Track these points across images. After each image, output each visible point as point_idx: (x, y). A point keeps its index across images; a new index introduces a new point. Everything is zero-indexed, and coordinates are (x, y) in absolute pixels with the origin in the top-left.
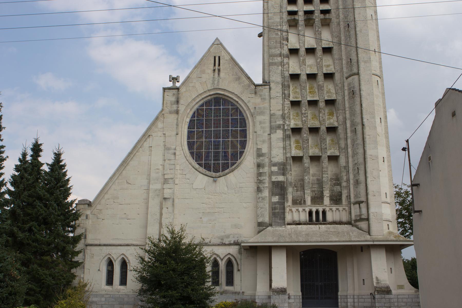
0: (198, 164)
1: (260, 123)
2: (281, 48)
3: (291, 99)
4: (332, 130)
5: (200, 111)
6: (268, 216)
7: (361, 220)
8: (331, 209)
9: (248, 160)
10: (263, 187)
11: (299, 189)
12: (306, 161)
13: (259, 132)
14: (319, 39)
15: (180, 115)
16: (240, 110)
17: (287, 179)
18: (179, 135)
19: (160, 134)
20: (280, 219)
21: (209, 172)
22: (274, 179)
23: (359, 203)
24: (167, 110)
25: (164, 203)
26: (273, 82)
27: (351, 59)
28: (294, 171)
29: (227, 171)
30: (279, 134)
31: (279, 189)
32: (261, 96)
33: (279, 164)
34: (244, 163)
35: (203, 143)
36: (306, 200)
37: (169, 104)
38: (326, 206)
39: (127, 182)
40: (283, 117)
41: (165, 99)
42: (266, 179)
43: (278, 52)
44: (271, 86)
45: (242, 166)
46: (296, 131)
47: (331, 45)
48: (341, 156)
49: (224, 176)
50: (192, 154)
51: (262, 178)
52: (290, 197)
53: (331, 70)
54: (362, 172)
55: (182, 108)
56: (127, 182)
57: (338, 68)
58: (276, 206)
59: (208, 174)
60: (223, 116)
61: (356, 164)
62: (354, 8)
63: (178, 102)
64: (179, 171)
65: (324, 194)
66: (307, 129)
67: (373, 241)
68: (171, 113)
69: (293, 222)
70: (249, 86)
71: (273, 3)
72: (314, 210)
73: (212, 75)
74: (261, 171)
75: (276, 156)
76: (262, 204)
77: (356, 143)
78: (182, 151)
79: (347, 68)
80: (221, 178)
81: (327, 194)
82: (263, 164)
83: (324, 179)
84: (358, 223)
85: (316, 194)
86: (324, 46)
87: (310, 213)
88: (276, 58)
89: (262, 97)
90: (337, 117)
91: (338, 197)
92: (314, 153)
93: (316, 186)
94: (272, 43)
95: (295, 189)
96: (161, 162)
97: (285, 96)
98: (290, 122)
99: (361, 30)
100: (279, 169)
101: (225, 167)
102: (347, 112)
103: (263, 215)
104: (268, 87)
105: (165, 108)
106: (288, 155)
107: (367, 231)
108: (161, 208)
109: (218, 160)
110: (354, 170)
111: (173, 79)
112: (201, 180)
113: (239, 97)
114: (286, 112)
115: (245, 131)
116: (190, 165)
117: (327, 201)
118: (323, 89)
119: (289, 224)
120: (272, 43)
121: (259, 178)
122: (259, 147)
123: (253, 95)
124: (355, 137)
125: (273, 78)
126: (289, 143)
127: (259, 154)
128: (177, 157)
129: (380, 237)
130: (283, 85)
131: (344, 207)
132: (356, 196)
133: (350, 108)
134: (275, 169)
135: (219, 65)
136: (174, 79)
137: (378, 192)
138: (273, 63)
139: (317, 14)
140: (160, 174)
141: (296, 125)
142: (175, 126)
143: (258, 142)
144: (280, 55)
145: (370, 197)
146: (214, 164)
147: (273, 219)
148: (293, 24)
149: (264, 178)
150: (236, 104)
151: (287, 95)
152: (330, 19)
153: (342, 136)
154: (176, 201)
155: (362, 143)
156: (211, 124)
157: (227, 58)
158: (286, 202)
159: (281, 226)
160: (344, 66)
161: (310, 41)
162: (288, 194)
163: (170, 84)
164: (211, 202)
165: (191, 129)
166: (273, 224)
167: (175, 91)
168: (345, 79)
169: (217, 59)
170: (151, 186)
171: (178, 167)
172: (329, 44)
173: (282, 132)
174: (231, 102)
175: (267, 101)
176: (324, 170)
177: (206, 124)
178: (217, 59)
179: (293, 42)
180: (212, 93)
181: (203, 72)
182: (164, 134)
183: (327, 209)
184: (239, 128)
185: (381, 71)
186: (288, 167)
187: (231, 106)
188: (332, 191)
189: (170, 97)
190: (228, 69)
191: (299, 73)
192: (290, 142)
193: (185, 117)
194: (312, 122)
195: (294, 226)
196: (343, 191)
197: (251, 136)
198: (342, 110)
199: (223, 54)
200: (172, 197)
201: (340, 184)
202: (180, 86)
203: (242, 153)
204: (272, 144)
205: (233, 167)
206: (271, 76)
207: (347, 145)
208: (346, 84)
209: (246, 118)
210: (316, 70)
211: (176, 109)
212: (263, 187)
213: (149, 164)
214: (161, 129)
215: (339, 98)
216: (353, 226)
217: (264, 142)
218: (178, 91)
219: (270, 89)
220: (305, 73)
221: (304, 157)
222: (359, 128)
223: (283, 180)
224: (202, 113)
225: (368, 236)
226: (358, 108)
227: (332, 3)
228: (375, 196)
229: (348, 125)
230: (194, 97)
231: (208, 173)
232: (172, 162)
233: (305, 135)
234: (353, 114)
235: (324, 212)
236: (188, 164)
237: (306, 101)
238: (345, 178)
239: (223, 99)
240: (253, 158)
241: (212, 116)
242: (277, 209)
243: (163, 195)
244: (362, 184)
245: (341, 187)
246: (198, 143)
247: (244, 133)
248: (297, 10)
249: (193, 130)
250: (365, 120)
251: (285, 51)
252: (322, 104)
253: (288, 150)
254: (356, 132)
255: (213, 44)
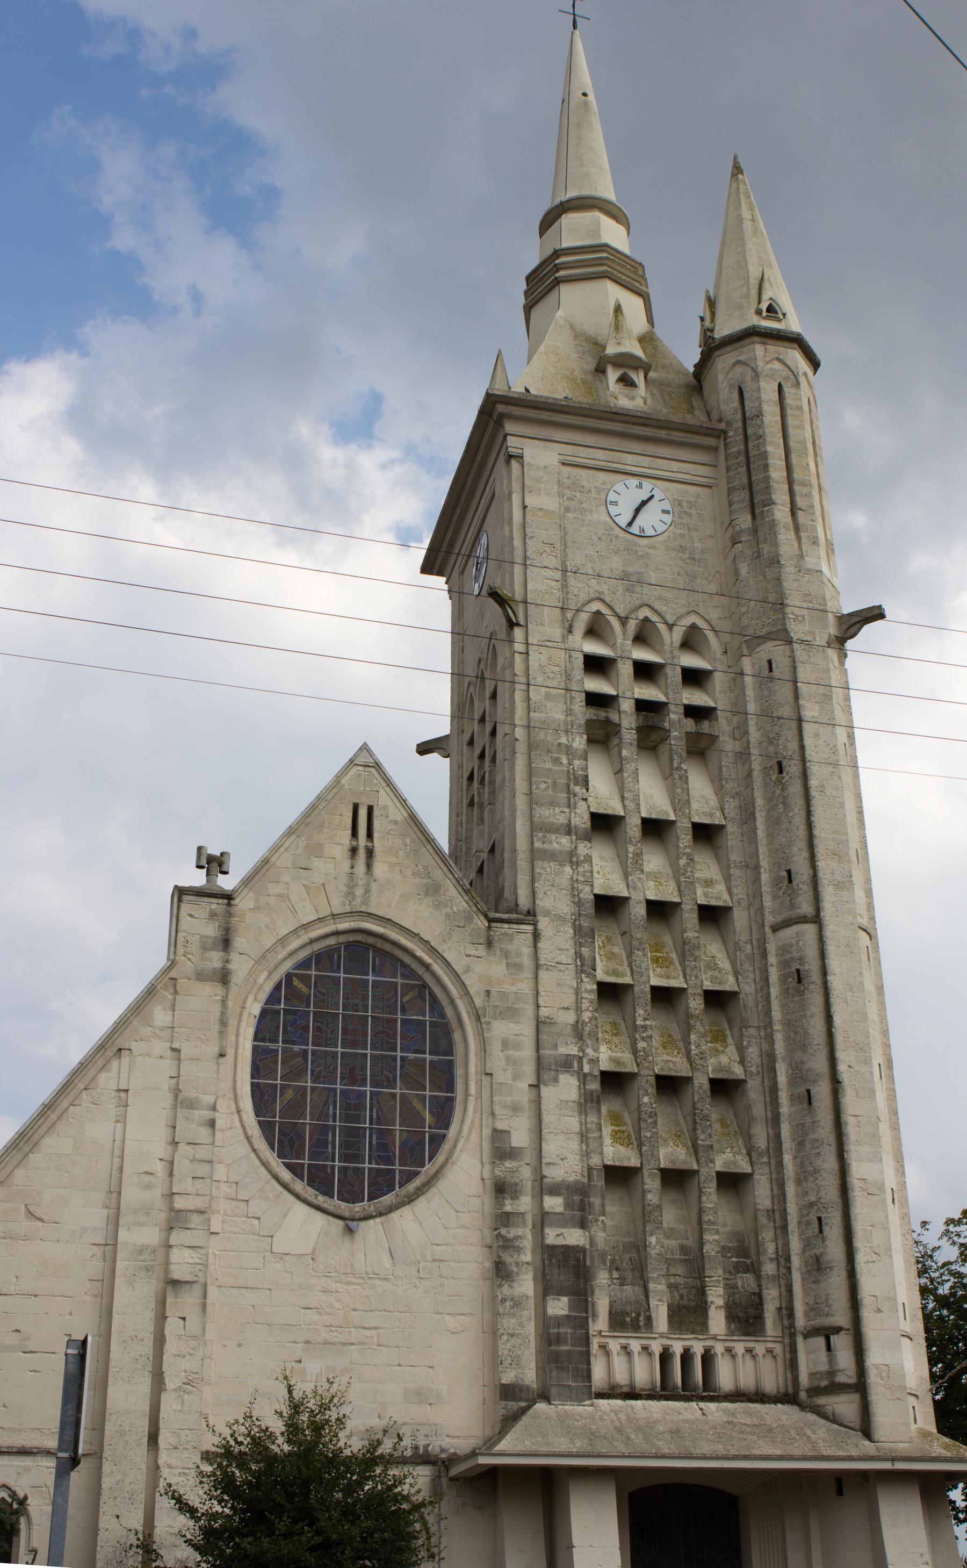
0: (289, 1166)
1: (505, 1044)
2: (569, 806)
3: (601, 976)
4: (724, 1088)
5: (296, 982)
6: (533, 1365)
7: (835, 1388)
8: (729, 1350)
9: (464, 1170)
10: (517, 1264)
11: (629, 1275)
12: (652, 1183)
13: (500, 1077)
14: (680, 800)
15: (234, 990)
16: (432, 994)
17: (592, 1241)
18: (229, 1058)
19: (160, 1047)
20: (575, 1378)
21: (329, 1200)
22: (552, 1236)
23: (828, 1333)
24: (186, 967)
25: (169, 1300)
26: (547, 913)
27: (789, 872)
28: (610, 1221)
29: (387, 1199)
30: (566, 1088)
31: (567, 1271)
32: (506, 955)
33: (568, 1187)
34: (450, 1176)
35: (305, 1094)
36: (654, 1315)
37: (194, 948)
38: (714, 1338)
39: (29, 1213)
40: (578, 1031)
41: (182, 926)
42: (524, 1234)
43: (562, 819)
44: (541, 926)
45: (443, 1185)
46: (614, 1081)
47: (718, 820)
48: (756, 1176)
49: (381, 1215)
50: (266, 1128)
51: (512, 1233)
52: (602, 1304)
53: (718, 895)
54: (834, 1232)
55: (240, 967)
56: (29, 1213)
57: (740, 892)
58: (562, 1330)
59: (325, 1206)
60: (374, 1007)
61: (812, 1204)
62: (800, 720)
63: (226, 943)
64: (223, 1186)
65: (710, 1299)
66: (652, 1080)
67: (893, 1460)
68: (200, 976)
69: (737, 1392)
70: (469, 919)
71: (544, 662)
72: (677, 1348)
73: (346, 865)
74: (508, 1208)
75: (557, 1161)
76: (513, 1321)
77: (811, 1136)
78: (236, 1117)
79: (775, 898)
80: (371, 1222)
81: (716, 1296)
82: (516, 1184)
83: (707, 1247)
84: (821, 1400)
85: (682, 1297)
86: (696, 819)
87: (665, 1357)
88: (553, 837)
89: (511, 960)
90: (741, 1050)
91: (751, 1311)
92: (673, 1161)
93: (680, 1270)
94: (543, 786)
95: (616, 1275)
96: (160, 1149)
97: (585, 966)
98: (596, 1050)
99: (823, 786)
100: (568, 1205)
101: (382, 1184)
102: (778, 1037)
103: (516, 1361)
104: (530, 928)
105: (180, 958)
106: (595, 1161)
107: (857, 1424)
108: (161, 1318)
109: (358, 1158)
110: (803, 1223)
111: (211, 859)
112: (302, 1225)
113: (433, 951)
114: (586, 1016)
115: (449, 1067)
116: (262, 1169)
117: (717, 1321)
118: (697, 953)
119: (601, 1395)
120: (543, 786)
121: (503, 1231)
122: (500, 1125)
123: (481, 951)
124: (808, 1120)
125: (543, 903)
126: (595, 1120)
127: (501, 1150)
128: (219, 1135)
129: (904, 1448)
130: (578, 930)
131: (770, 1345)
132: (813, 1309)
133: (788, 1024)
134: (554, 1203)
135: (370, 835)
136: (214, 864)
137: (889, 1299)
138: (545, 851)
139: (675, 714)
140: (158, 1192)
141: (616, 1061)
142: (216, 1028)
143: (498, 1110)
144: (568, 830)
145: (867, 1314)
146: (343, 1170)
147: (554, 1374)
148: (602, 736)
149: (519, 1232)
150: (421, 971)
151: (588, 963)
152: (713, 738)
153: (759, 1110)
154: (212, 1292)
155: (832, 1139)
156: (334, 1031)
157: (398, 814)
158: (590, 1320)
159: (580, 1401)
160: (766, 889)
161: (652, 794)
162: (597, 1292)
163: (198, 879)
164: (338, 1305)
165: (263, 1040)
166: (554, 1391)
167: (217, 905)
168: (768, 930)
169: (363, 813)
170: (123, 1235)
171: (220, 1172)
172: (711, 815)
173: (577, 1083)
174: (404, 965)
175: (528, 974)
176: (706, 1218)
177: (317, 1029)
178: (363, 813)
179: (602, 793)
180: (343, 926)
181: (316, 851)
182: (173, 1050)
183: (719, 1348)
184: (428, 1057)
185: (872, 919)
186: (596, 1201)
187: (404, 976)
188: (730, 1288)
189: (201, 923)
190: (401, 854)
191: (625, 893)
192: (600, 1118)
193: (251, 998)
194: (665, 1057)
195: (619, 1402)
196: (765, 1292)
197: (472, 1085)
198: (758, 1028)
199: (383, 799)
200: (202, 1280)
201: (754, 1269)
202: (235, 890)
203: (437, 1141)
204: (546, 1118)
205: (412, 1186)
206: (540, 895)
207: (781, 1144)
208: (771, 947)
209: (454, 1024)
210: (676, 893)
211: (218, 964)
212: (517, 1264)
213: (117, 1152)
214: (162, 1029)
215: (748, 989)
216: (802, 1407)
217: (515, 1108)
218: (229, 905)
219: (536, 936)
220: (642, 898)
221: (646, 1172)
222: (822, 1091)
223: (581, 1244)
224: (304, 990)
225: (867, 1443)
226: (817, 1027)
227: (718, 688)
228: (879, 1311)
229: (782, 1078)
230: (283, 931)
231: (321, 1200)
232: (202, 1153)
233: (646, 1099)
234: (798, 1041)
235: (708, 1358)
236: (258, 1163)
237: (648, 989)
238: (770, 1248)
239: (379, 952)
240: (477, 1163)
241: (337, 1004)
242: (565, 1342)
243: (167, 1271)
244: (835, 1272)
245: (758, 1277)
246: (289, 1094)
247: (445, 1077)
248: (614, 693)
249: (272, 1046)
250: (842, 1067)
251: (581, 820)
252: (696, 1004)
253: (593, 1145)
254: (810, 1103)
255: (351, 761)
